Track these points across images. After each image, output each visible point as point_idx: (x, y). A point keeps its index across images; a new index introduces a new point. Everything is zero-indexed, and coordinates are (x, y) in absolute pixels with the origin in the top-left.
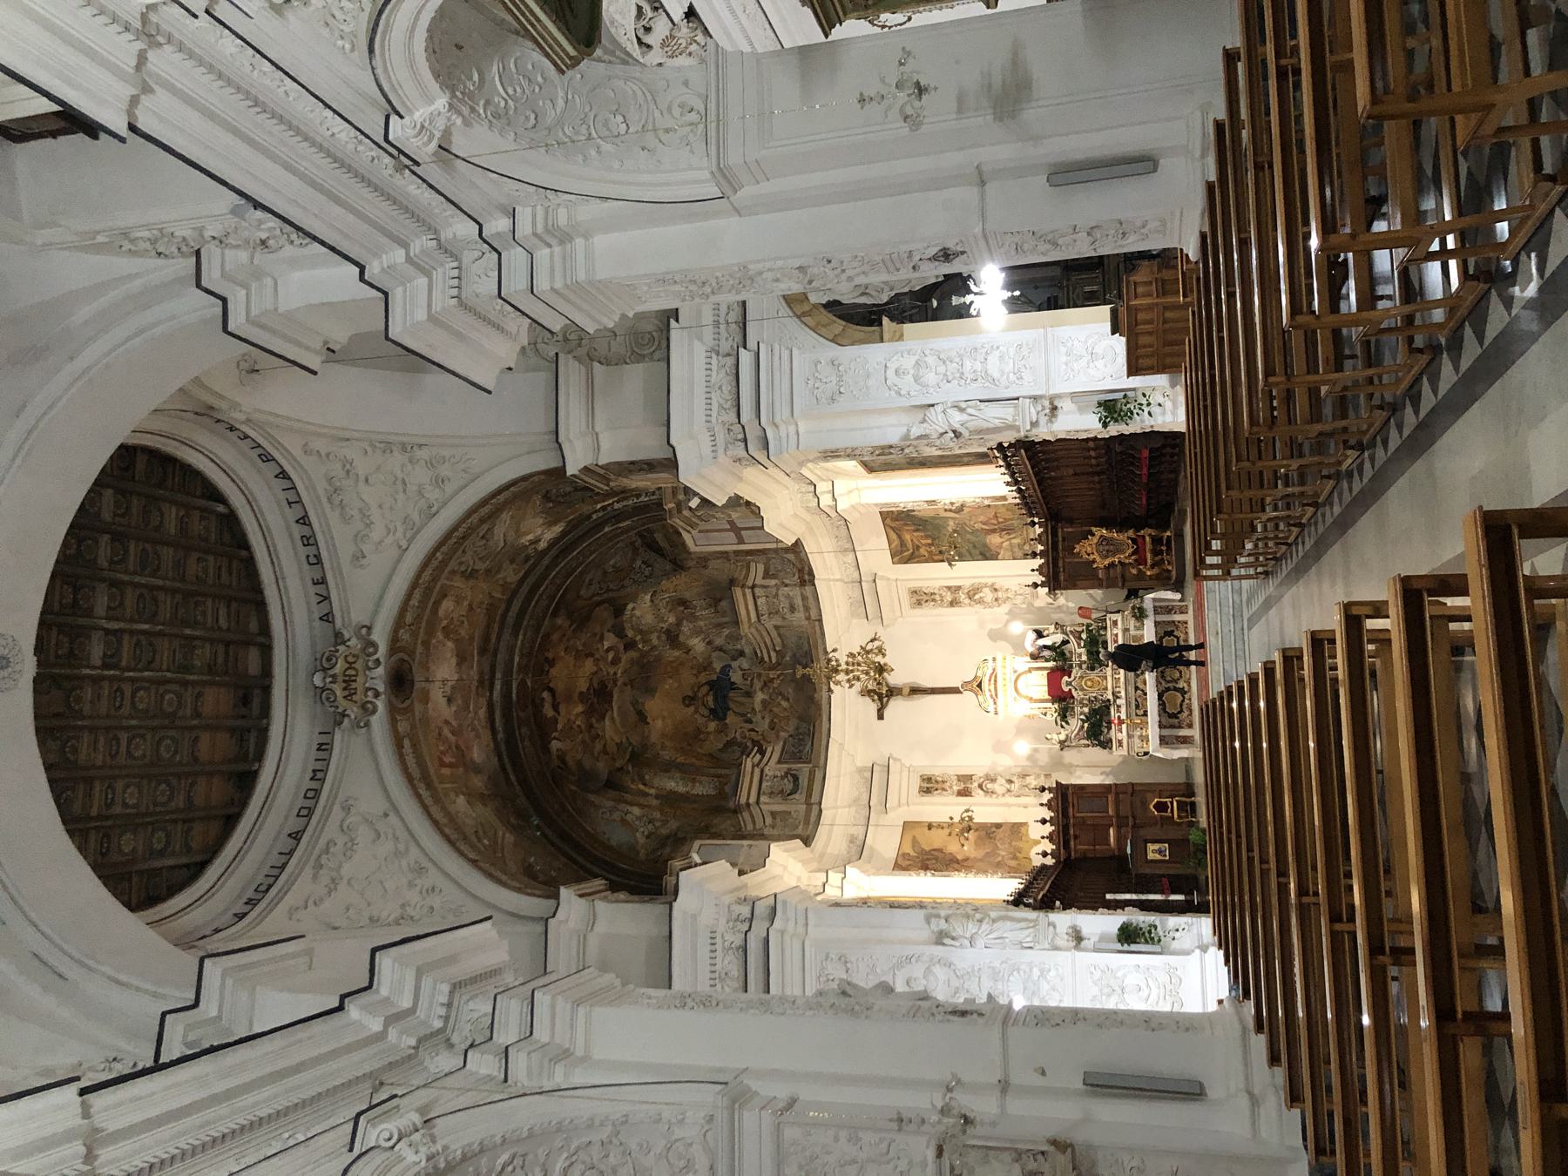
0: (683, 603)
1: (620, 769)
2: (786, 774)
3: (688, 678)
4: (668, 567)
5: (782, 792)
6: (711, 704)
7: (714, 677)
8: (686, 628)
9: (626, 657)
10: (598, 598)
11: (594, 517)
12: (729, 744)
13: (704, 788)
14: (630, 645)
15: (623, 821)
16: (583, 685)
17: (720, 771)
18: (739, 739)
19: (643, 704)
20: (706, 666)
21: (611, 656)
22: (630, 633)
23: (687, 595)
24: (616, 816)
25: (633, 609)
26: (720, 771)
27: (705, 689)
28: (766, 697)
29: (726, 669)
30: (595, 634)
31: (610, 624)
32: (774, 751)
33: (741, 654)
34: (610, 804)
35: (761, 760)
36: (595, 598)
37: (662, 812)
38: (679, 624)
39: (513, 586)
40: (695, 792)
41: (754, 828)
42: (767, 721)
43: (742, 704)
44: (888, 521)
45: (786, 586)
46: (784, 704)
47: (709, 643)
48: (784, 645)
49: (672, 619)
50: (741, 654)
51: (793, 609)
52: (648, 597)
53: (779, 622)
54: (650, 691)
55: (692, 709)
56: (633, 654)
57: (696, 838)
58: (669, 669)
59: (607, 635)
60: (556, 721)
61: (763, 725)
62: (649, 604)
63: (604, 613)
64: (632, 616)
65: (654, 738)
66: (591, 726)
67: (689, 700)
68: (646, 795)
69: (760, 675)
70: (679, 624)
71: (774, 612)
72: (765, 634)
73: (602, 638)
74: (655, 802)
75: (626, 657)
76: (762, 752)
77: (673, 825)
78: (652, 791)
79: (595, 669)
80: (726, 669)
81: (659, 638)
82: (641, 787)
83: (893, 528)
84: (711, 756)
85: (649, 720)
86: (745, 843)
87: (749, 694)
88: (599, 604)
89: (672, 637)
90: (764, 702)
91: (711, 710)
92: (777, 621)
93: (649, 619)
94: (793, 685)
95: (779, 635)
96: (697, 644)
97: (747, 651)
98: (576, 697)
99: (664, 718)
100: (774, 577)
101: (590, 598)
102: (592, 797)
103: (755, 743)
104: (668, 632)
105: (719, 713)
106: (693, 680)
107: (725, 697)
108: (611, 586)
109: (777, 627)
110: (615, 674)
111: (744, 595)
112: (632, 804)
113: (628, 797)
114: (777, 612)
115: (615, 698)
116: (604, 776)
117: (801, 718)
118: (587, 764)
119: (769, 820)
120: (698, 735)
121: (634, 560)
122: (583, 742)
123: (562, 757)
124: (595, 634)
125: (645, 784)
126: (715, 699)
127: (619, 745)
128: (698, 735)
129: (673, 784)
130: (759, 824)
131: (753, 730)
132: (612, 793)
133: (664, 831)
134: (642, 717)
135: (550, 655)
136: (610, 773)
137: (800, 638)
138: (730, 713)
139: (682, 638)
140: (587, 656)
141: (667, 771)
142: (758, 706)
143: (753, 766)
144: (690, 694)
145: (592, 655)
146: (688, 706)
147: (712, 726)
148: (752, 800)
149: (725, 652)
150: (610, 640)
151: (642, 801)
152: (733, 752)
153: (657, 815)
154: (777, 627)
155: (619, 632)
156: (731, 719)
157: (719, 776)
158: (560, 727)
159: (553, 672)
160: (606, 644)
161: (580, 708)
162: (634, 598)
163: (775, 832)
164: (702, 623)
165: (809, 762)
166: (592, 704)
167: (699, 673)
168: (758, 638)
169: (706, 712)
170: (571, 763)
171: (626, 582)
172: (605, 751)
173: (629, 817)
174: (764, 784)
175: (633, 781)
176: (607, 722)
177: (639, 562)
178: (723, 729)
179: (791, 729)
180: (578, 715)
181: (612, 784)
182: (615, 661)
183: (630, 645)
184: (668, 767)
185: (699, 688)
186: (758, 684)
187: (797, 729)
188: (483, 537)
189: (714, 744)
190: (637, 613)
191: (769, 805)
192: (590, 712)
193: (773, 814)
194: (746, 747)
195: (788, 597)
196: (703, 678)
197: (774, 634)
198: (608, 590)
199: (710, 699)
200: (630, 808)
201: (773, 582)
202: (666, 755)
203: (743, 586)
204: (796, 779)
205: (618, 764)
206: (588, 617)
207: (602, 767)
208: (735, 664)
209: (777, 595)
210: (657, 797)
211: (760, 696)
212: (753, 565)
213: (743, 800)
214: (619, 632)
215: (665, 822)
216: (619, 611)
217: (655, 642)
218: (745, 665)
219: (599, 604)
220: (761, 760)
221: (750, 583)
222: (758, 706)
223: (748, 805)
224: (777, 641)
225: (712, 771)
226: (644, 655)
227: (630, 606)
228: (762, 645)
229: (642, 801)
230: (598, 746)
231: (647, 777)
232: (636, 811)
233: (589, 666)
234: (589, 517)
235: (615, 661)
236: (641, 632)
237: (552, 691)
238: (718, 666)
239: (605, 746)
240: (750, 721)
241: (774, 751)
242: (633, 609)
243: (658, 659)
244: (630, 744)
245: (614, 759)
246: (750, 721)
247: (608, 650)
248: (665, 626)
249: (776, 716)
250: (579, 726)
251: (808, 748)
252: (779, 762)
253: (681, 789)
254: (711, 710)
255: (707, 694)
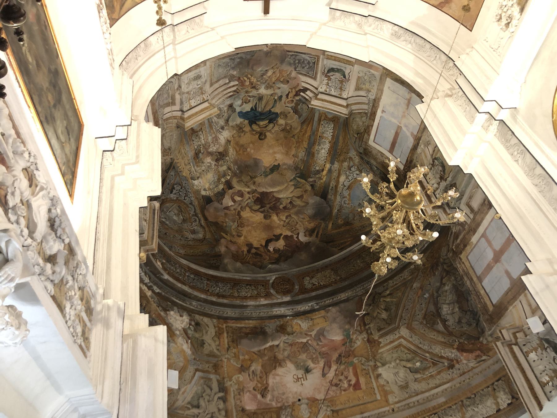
0: (197, 155)
1: (312, 186)
2: (326, 76)
3: (246, 138)
4: (172, 173)
5: (341, 82)
6: (266, 122)
7: (247, 122)
8: (213, 149)
9: (238, 187)
10: (203, 222)
11: (158, 291)
12: (296, 111)
13: (328, 131)
14: (229, 185)
15: (349, 188)
16: (258, 217)
17: (316, 119)
18: (293, 105)
19: (266, 168)
20: (240, 128)
21: (238, 198)
22: (221, 187)
23: (191, 154)
24: (346, 193)
25: (205, 190)
26: (316, 119)
27: (255, 127)
28: (263, 86)
29: (242, 115)
30: (226, 214)
31: (216, 204)
32: (305, 81)
33: (231, 106)
34: (338, 198)
35: (311, 91)
36: (203, 224)
37: (343, 161)
38: (210, 154)
39: (215, 321)
40: (330, 138)
41: (368, 104)
42: (282, 85)
43: (267, 103)
44: (115, 16)
45: (180, 87)
46: (270, 73)
47: (223, 128)
48: (225, 77)
49: (208, 160)
50: (231, 106)
51: (198, 77)
52: (196, 182)
53: (208, 85)
54: (257, 162)
55: (268, 134)
56: (234, 182)
57: (366, 143)
58: (241, 152)
59: (224, 205)
60: (286, 237)
61: (285, 88)
62: (200, 180)
63: (211, 211)
64: (210, 189)
65: (290, 161)
66: (285, 208)
67: (262, 136)
68: (330, 171)
69: (247, 92)
70: (210, 154)
71: (201, 91)
72: (216, 92)
73: (227, 208)
74: (336, 165)
75: (238, 187)
76: (305, 90)
77: (353, 154)
78: (328, 166)
79: (247, 208)
80: (242, 115)
81: (222, 166)
82: (325, 172)
83: (122, 5)
84: (303, 123)
85: (276, 164)
86: (379, 113)
87: (260, 98)
88: (206, 219)
89: (220, 156)
90: (267, 88)
91: (269, 122)
92: (207, 87)
93: (210, 176)
94: (255, 68)
95: (217, 82)
96: (225, 135)
97: (228, 102)
98: (268, 221)
99: (275, 153)
100: (173, 98)
101: (204, 228)
102: (335, 211)
103: (297, 94)
104: (217, 160)
105: (272, 117)
106: (248, 135)
107: (261, 114)
108: (192, 213)
109: (211, 85)
110: (249, 193)
111: (189, 117)
112: (338, 182)
113: (333, 184)
114: (201, 88)
115: (264, 190)
116: (318, 198)
117: (282, 61)
118: (310, 211)
119: (362, 93)
120: (287, 130)
121: (172, 200)
122: (297, 213)
123: (310, 232)
124: (226, 214)
125: (323, 170)
126: (263, 120)
127: (296, 187)
128: (287, 130)
129: (323, 151)
130: (365, 100)
131: (287, 95)
132: (330, 196)
133: (357, 160)
134: (275, 168)
135: (245, 249)
136: (316, 194)
137: (219, 65)
138: (273, 110)
139: (221, 150)
140: (240, 217)
141: (313, 155)
142: (269, 92)
143: (317, 99)
144: (257, 136)
145: (239, 212)
146: (265, 136)
147: (281, 121)
148: (344, 103)
149: (229, 118)
150: (227, 201)
151: (335, 174)
152: (302, 109)
153: (346, 164)
154: (211, 85)
155: (221, 195)
156: (277, 109)
157: (320, 120)
158: (289, 234)
159: (256, 244)
160: (231, 203)
161: (275, 218)
162: (198, 192)
163: (374, 91)
164: (210, 138)
165: (318, 57)
166: (270, 208)
167: (243, 131)
168: (220, 96)
169: (271, 125)
170: (312, 225)
171: (187, 201)
172: (300, 197)
173: (347, 184)
174: (333, 93)
175: (320, 178)
176: (281, 196)
177: (172, 196)
178: (285, 115)
179: (291, 69)
180: (280, 220)
181: (324, 194)
182: (241, 195)
183: (229, 185)
184: (310, 154)
185: (254, 131)
186: (254, 92)
187: (290, 64)
188: (198, 407)
189: (294, 121)
190: (207, 186)
191: (350, 90)
192: (275, 209)
193: (358, 88)
194: (300, 100)
195: (189, 84)
196: (247, 129)
197: (216, 85)
198: (196, 215)
199: (262, 123)
200: (341, 183)
201: (178, 97)
202: (302, 154)
203: (182, 118)
204: (332, 70)
205: (309, 188)
206: (216, 224)
207: (313, 200)
208: (238, 109)
209: (188, 93)
210: (332, 163)
211: (263, 91)
212: (165, 117)
213: (345, 111)
214: (221, 195)
215: (351, 158)
216: (208, 200)
217: (225, 168)
218: (240, 102)
219: (206, 219)
220: (311, 91)
221: (179, 114)
222: (269, 92)
223: (347, 106)
224: (221, 82)
225: (315, 123)
226: (235, 174)
227: (203, 193)
228: (225, 92)
229: (335, 174)
230: (298, 202)
231: (317, 168)
232: (342, 179)
233: (246, 214)
234: (158, 294)
235: (241, 195)
236: (219, 180)
237: (268, 242)
238: (239, 120)
239: (298, 197)
240: (280, 98)
241: (305, 81)
242: (205, 190)
243: (235, 162)
244: (294, 178)
245: (306, 191)
246: (280, 98)
247: (234, 201)
248: (213, 163)
249: (278, 80)
250: (287, 218)
251: (306, 57)
252: (315, 79)
253: (327, 146)
254: (269, 122)
255: (259, 125)
